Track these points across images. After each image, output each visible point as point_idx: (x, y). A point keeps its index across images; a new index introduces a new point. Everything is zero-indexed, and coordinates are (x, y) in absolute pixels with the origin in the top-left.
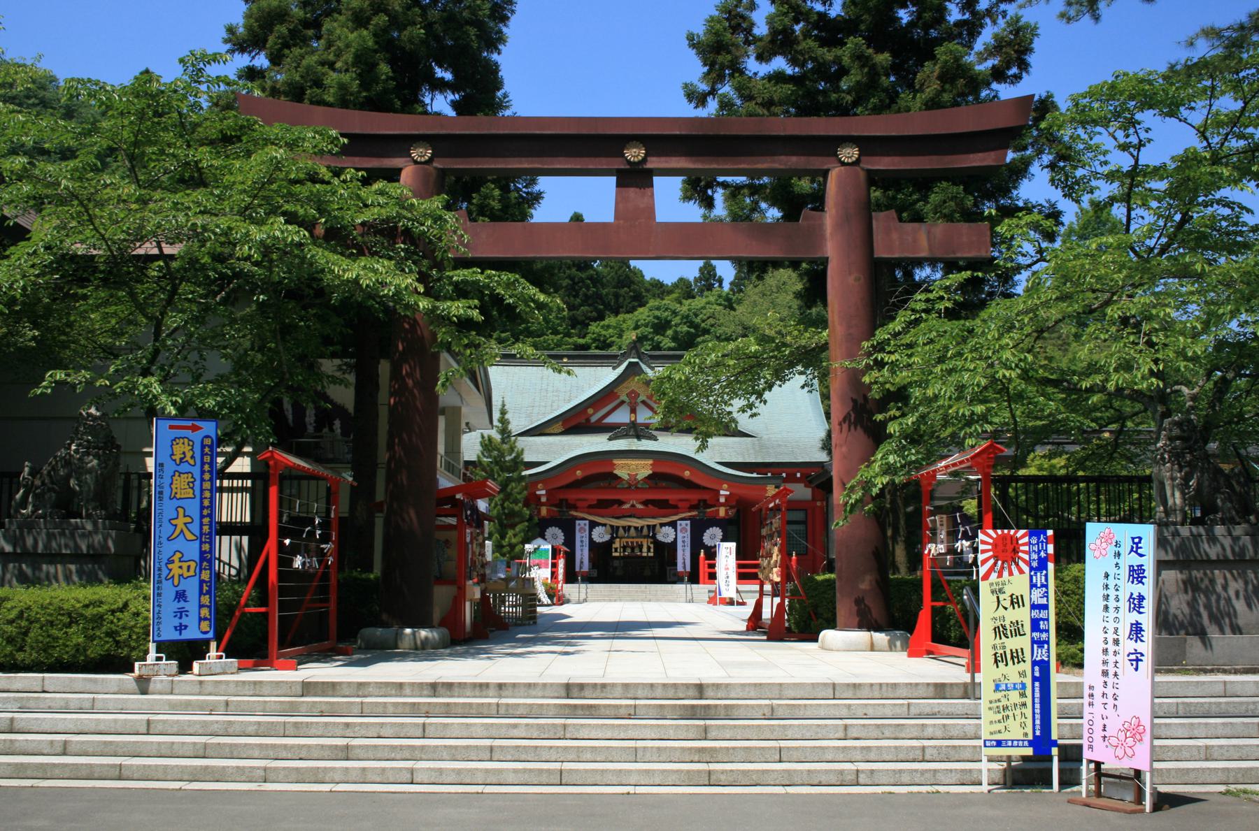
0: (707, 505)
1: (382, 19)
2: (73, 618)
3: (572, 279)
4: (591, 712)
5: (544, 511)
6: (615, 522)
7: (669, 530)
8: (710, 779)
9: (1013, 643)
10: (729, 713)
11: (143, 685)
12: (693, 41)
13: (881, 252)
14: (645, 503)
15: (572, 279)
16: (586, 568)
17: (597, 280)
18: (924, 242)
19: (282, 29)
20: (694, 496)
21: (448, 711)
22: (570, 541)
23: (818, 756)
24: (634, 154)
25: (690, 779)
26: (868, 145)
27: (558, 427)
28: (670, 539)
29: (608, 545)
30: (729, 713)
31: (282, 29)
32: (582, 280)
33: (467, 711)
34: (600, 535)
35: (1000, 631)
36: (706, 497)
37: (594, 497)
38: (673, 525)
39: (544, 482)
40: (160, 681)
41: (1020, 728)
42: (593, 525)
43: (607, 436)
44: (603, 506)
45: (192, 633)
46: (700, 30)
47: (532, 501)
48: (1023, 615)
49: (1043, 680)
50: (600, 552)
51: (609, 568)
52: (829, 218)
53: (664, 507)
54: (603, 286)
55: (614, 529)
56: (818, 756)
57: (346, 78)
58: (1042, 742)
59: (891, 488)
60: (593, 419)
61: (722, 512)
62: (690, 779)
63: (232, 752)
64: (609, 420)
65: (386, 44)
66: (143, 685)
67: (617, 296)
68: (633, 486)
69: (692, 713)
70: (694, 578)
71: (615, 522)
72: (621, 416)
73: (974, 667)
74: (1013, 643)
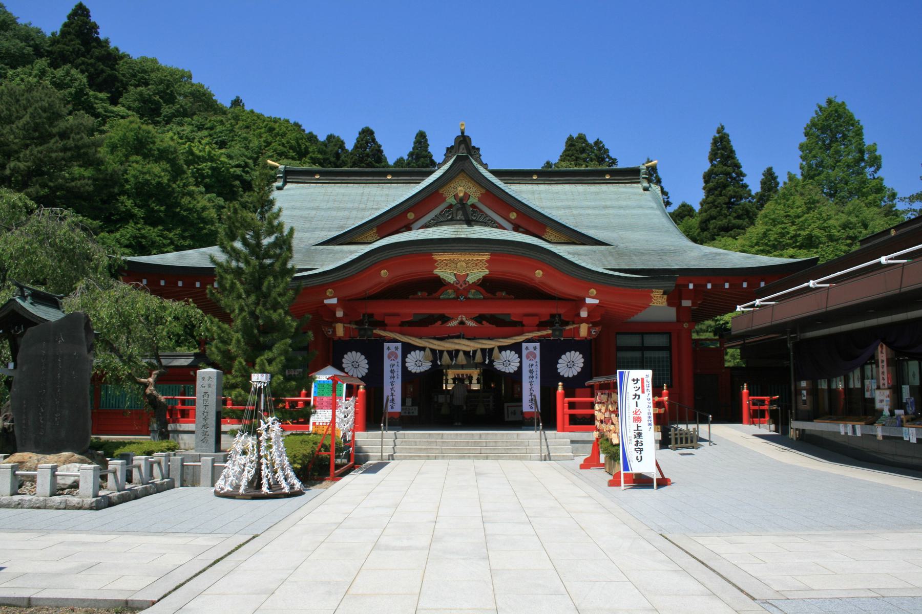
6: (437, 345)
7: (511, 355)
14: (479, 319)
16: (398, 408)
28: (512, 368)
34: (418, 363)
38: (517, 348)
42: (408, 349)
44: (423, 324)
53: (501, 324)
68: (461, 291)
71: (437, 345)
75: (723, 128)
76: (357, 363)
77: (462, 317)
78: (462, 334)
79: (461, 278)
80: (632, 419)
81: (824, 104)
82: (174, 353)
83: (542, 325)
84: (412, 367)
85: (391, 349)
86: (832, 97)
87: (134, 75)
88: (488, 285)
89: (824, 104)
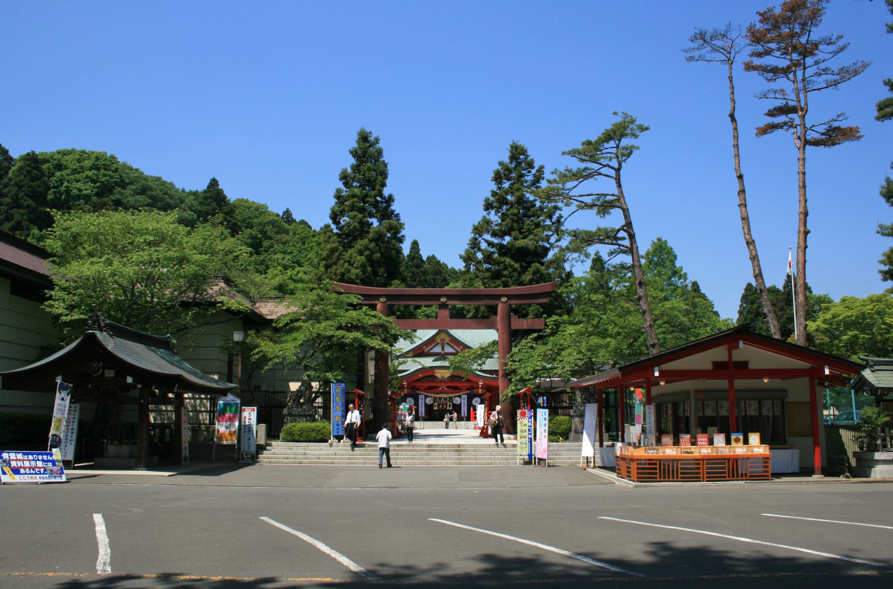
0: (474, 388)
1: (367, 252)
2: (313, 430)
3: (413, 272)
4: (434, 450)
5: (406, 391)
6: (436, 396)
7: (458, 399)
8: (460, 464)
9: (524, 434)
10: (465, 451)
11: (331, 445)
12: (461, 257)
13: (513, 327)
14: (448, 387)
15: (413, 272)
16: (423, 415)
17: (425, 273)
18: (525, 324)
19: (337, 254)
20: (468, 385)
21: (402, 450)
22: (416, 404)
23: (484, 459)
24: (443, 300)
25: (456, 463)
26: (508, 296)
27: (411, 354)
28: (458, 403)
29: (432, 405)
30: (465, 451)
31: (337, 254)
32: (418, 273)
33: (406, 451)
34: (429, 401)
35: (522, 431)
36: (473, 385)
37: (427, 385)
38: (460, 396)
39: (406, 380)
40: (335, 444)
41: (526, 452)
42: (426, 397)
43: (433, 358)
44: (430, 389)
45: (340, 434)
46: (463, 253)
47: (402, 387)
48: (527, 428)
49: (531, 442)
50: (429, 408)
51: (433, 415)
52: (499, 317)
53: (456, 389)
54: (428, 274)
55: (435, 399)
56: (484, 459)
57: (357, 271)
58: (530, 455)
59: (512, 396)
60: (426, 350)
61: (480, 391)
62: (456, 463)
63: (356, 459)
64: (432, 351)
65: (369, 259)
66: (331, 445)
67: (434, 279)
68: (443, 381)
69: (457, 451)
70: (468, 419)
71: (436, 396)
72: (438, 349)
73: (516, 439)
74: (524, 434)
75: (598, 252)
76: (411, 401)
77: (443, 387)
78: (443, 392)
79: (443, 377)
80: (693, 448)
81: (656, 241)
82: (604, 431)
83: (468, 389)
84: (428, 402)
85: (421, 397)
86: (659, 236)
87: (244, 221)
88: (452, 376)
89: (656, 241)
